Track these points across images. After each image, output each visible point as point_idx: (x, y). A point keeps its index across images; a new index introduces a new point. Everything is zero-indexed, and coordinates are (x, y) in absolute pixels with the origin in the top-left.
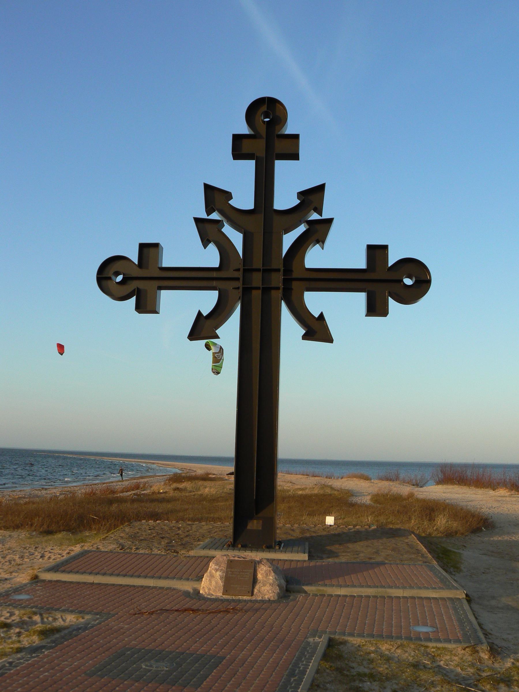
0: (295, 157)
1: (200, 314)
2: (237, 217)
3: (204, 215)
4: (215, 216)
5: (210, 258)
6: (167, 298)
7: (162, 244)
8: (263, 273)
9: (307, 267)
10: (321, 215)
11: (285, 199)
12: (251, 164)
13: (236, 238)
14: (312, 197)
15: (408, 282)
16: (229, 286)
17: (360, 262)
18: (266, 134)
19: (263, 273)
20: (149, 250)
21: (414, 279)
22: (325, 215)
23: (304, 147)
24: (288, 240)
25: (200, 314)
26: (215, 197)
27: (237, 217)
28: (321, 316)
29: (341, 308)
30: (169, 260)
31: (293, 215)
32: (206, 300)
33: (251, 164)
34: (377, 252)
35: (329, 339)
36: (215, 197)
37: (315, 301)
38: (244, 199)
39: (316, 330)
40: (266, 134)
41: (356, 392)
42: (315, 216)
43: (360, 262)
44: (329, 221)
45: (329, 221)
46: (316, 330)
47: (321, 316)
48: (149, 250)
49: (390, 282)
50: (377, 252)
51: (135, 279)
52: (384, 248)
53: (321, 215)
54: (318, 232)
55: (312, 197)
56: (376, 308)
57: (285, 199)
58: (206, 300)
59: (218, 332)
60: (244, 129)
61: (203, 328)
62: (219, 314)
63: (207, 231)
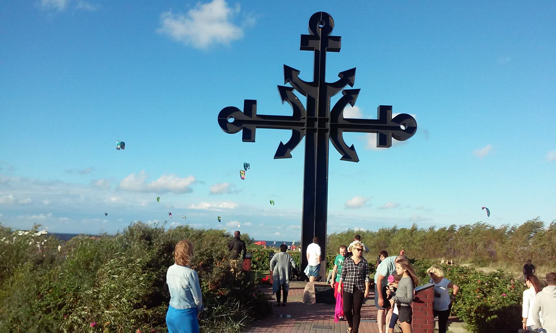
0: (338, 50)
1: (281, 143)
2: (301, 86)
3: (282, 84)
4: (288, 85)
5: (287, 110)
6: (260, 133)
7: (257, 102)
8: (317, 123)
9: (344, 117)
10: (352, 85)
11: (331, 77)
12: (312, 54)
13: (303, 100)
14: (348, 76)
15: (403, 127)
16: (298, 128)
17: (374, 116)
18: (321, 36)
19: (317, 123)
20: (250, 104)
21: (407, 127)
22: (354, 88)
23: (343, 44)
24: (334, 100)
25: (281, 143)
26: (290, 73)
27: (301, 86)
28: (353, 146)
29: (365, 142)
30: (261, 110)
31: (338, 85)
32: (286, 135)
33: (312, 54)
34: (385, 110)
35: (356, 159)
36: (290, 73)
37: (349, 138)
38: (307, 75)
39: (349, 154)
40: (321, 36)
41: (372, 192)
42: (348, 87)
43: (374, 116)
44: (357, 91)
45: (357, 91)
46: (349, 154)
47: (353, 146)
48: (250, 104)
49: (391, 127)
50: (385, 110)
51: (242, 121)
52: (390, 108)
53: (352, 85)
54: (350, 97)
55: (348, 76)
56: (383, 142)
57: (331, 77)
58: (286, 135)
59: (292, 153)
60: (307, 32)
61: (283, 152)
62: (293, 143)
63: (284, 93)
